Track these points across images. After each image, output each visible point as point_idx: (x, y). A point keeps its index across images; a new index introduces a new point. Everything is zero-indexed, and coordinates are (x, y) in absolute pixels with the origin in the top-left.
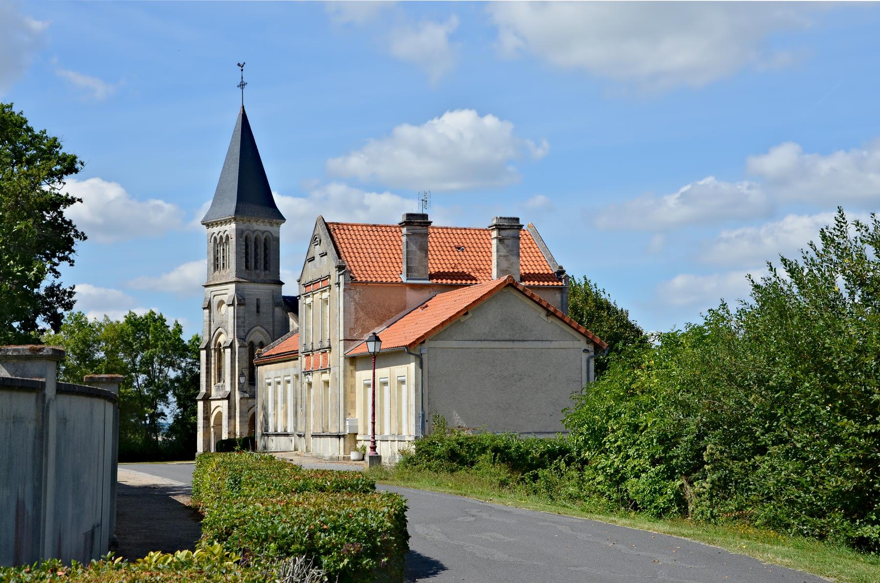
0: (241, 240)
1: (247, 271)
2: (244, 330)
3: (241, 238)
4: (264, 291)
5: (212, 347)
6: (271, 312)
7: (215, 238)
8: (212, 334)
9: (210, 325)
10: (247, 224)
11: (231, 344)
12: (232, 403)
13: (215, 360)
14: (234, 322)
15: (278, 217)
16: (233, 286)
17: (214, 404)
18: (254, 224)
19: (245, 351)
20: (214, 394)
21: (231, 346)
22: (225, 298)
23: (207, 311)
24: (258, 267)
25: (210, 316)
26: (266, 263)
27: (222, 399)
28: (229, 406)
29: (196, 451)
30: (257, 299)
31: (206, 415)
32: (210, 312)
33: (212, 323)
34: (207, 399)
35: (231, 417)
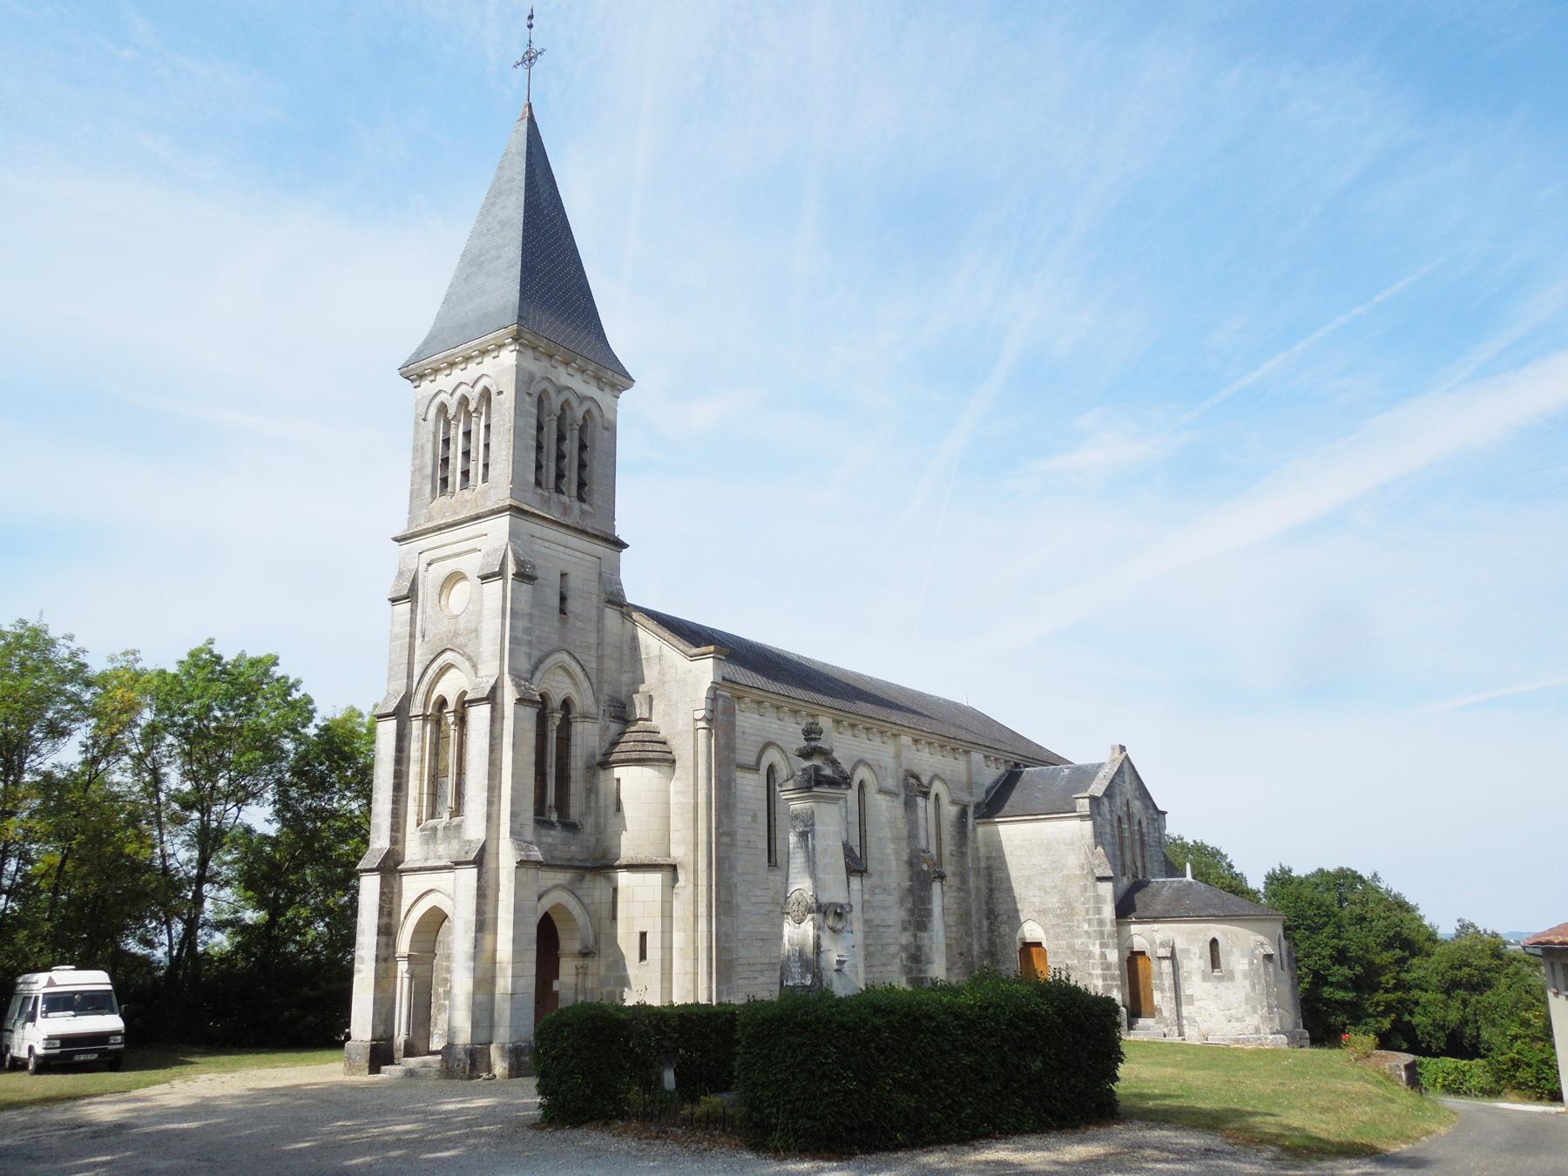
1: (539, 491)
2: (529, 655)
5: (416, 709)
6: (594, 618)
7: (443, 408)
8: (416, 679)
9: (411, 647)
10: (545, 362)
11: (494, 689)
12: (490, 876)
13: (423, 749)
14: (503, 625)
15: (615, 377)
16: (504, 521)
17: (411, 886)
19: (530, 713)
20: (413, 852)
21: (492, 697)
22: (472, 565)
25: (413, 622)
26: (582, 485)
28: (479, 888)
29: (557, 977)
30: (563, 575)
31: (385, 920)
32: (413, 612)
33: (418, 641)
34: (391, 868)
35: (484, 923)
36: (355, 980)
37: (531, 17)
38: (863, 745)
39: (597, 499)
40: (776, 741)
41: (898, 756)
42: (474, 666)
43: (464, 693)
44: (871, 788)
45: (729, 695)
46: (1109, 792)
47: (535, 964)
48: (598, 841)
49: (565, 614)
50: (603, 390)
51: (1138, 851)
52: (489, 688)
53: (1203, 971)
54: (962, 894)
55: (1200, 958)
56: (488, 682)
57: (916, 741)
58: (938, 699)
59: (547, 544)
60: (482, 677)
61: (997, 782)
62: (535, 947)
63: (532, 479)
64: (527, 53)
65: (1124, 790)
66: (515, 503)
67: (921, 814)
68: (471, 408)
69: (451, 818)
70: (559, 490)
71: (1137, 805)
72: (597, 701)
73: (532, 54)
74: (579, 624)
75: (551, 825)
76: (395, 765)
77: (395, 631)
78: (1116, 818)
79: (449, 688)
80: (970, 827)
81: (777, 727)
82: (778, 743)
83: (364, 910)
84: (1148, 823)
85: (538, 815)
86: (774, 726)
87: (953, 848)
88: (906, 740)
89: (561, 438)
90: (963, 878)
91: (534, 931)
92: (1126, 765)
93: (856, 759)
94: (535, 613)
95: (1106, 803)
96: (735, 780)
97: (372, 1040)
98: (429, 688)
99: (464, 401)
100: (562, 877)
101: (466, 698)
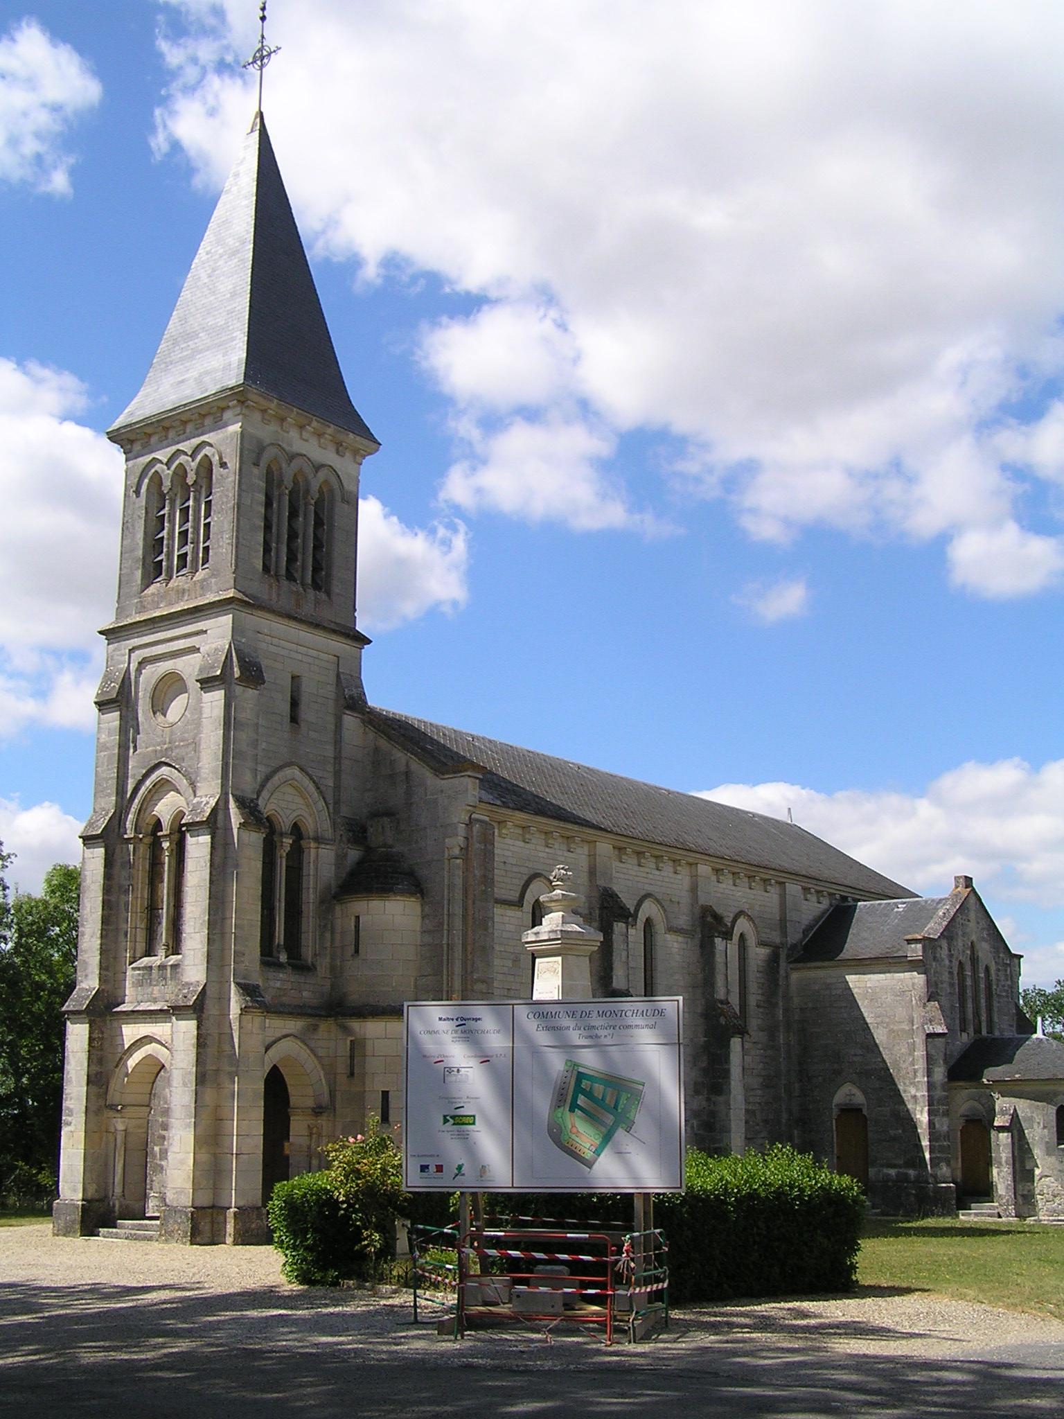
0: (256, 471)
3: (256, 464)
4: (314, 653)
10: (273, 427)
18: (294, 434)
21: (214, 823)
22: (189, 667)
23: (113, 718)
24: (297, 575)
27: (175, 1011)
31: (95, 1068)
36: (63, 1133)
37: (263, 9)
38: (651, 876)
39: (336, 588)
40: (543, 873)
41: (694, 889)
42: (193, 785)
43: (181, 814)
44: (660, 927)
45: (487, 819)
46: (949, 933)
47: (262, 1122)
48: (333, 986)
49: (297, 723)
50: (343, 456)
51: (983, 1001)
52: (209, 811)
53: (1047, 1143)
54: (769, 1052)
55: (1045, 1127)
56: (208, 803)
57: (717, 871)
58: (754, 815)
59: (275, 641)
60: (201, 797)
61: (817, 920)
62: (262, 1103)
63: (259, 565)
64: (258, 51)
65: (968, 930)
66: (240, 596)
67: (719, 959)
68: (190, 481)
69: (166, 957)
70: (290, 577)
71: (984, 950)
72: (334, 825)
73: (265, 53)
74: (313, 735)
75: (279, 966)
76: (103, 894)
77: (101, 741)
78: (956, 964)
79: (165, 809)
80: (782, 972)
81: (545, 855)
82: (656, 895)
83: (71, 1057)
84: (998, 970)
85: (265, 956)
86: (541, 854)
87: (759, 998)
88: (704, 869)
89: (293, 514)
90: (771, 1032)
91: (261, 1086)
92: (972, 900)
93: (643, 893)
94: (261, 722)
95: (944, 944)
96: (493, 918)
97: (83, 1200)
98: (141, 807)
99: (181, 472)
100: (293, 1025)
101: (183, 822)
